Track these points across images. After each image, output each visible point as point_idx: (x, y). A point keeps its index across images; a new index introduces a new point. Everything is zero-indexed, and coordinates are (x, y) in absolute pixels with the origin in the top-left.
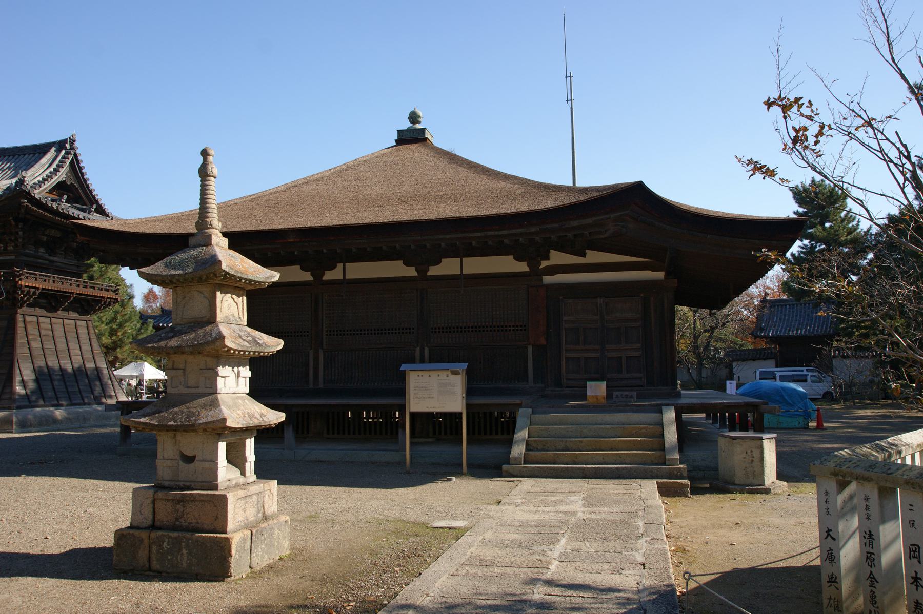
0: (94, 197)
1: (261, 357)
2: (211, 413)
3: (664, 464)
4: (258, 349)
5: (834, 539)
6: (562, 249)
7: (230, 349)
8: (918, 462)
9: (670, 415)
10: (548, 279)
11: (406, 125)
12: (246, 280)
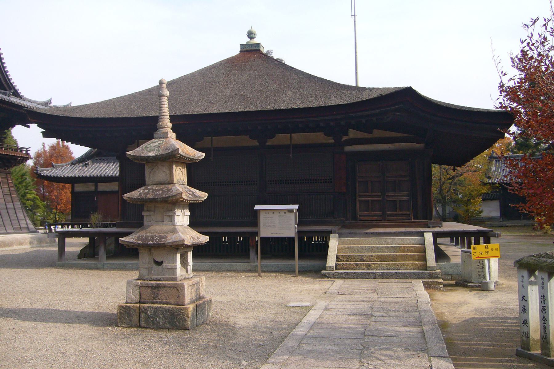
0: (11, 84)
1: (195, 203)
2: (174, 236)
3: (427, 270)
4: (196, 199)
5: (526, 301)
6: (357, 128)
7: (184, 199)
8: (406, 193)
9: (429, 237)
10: (348, 149)
11: (245, 40)
12: (189, 158)
